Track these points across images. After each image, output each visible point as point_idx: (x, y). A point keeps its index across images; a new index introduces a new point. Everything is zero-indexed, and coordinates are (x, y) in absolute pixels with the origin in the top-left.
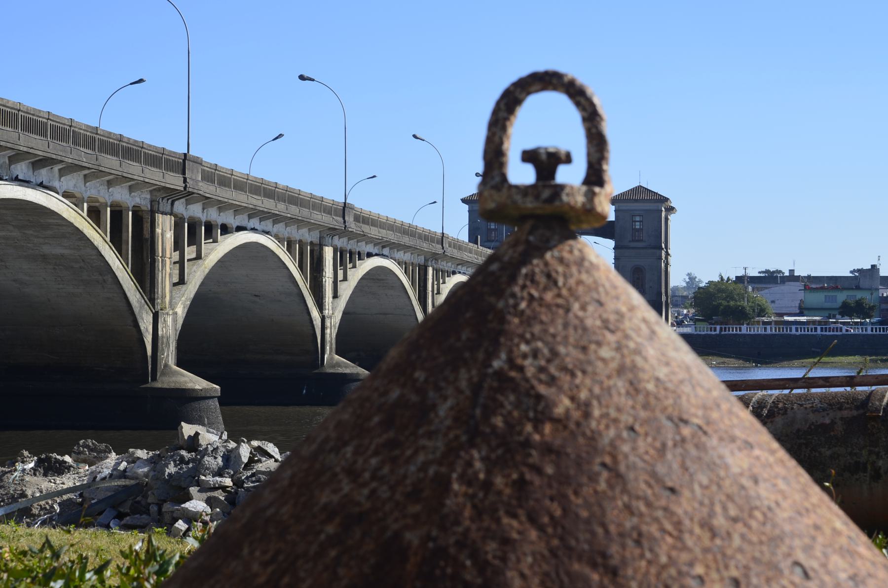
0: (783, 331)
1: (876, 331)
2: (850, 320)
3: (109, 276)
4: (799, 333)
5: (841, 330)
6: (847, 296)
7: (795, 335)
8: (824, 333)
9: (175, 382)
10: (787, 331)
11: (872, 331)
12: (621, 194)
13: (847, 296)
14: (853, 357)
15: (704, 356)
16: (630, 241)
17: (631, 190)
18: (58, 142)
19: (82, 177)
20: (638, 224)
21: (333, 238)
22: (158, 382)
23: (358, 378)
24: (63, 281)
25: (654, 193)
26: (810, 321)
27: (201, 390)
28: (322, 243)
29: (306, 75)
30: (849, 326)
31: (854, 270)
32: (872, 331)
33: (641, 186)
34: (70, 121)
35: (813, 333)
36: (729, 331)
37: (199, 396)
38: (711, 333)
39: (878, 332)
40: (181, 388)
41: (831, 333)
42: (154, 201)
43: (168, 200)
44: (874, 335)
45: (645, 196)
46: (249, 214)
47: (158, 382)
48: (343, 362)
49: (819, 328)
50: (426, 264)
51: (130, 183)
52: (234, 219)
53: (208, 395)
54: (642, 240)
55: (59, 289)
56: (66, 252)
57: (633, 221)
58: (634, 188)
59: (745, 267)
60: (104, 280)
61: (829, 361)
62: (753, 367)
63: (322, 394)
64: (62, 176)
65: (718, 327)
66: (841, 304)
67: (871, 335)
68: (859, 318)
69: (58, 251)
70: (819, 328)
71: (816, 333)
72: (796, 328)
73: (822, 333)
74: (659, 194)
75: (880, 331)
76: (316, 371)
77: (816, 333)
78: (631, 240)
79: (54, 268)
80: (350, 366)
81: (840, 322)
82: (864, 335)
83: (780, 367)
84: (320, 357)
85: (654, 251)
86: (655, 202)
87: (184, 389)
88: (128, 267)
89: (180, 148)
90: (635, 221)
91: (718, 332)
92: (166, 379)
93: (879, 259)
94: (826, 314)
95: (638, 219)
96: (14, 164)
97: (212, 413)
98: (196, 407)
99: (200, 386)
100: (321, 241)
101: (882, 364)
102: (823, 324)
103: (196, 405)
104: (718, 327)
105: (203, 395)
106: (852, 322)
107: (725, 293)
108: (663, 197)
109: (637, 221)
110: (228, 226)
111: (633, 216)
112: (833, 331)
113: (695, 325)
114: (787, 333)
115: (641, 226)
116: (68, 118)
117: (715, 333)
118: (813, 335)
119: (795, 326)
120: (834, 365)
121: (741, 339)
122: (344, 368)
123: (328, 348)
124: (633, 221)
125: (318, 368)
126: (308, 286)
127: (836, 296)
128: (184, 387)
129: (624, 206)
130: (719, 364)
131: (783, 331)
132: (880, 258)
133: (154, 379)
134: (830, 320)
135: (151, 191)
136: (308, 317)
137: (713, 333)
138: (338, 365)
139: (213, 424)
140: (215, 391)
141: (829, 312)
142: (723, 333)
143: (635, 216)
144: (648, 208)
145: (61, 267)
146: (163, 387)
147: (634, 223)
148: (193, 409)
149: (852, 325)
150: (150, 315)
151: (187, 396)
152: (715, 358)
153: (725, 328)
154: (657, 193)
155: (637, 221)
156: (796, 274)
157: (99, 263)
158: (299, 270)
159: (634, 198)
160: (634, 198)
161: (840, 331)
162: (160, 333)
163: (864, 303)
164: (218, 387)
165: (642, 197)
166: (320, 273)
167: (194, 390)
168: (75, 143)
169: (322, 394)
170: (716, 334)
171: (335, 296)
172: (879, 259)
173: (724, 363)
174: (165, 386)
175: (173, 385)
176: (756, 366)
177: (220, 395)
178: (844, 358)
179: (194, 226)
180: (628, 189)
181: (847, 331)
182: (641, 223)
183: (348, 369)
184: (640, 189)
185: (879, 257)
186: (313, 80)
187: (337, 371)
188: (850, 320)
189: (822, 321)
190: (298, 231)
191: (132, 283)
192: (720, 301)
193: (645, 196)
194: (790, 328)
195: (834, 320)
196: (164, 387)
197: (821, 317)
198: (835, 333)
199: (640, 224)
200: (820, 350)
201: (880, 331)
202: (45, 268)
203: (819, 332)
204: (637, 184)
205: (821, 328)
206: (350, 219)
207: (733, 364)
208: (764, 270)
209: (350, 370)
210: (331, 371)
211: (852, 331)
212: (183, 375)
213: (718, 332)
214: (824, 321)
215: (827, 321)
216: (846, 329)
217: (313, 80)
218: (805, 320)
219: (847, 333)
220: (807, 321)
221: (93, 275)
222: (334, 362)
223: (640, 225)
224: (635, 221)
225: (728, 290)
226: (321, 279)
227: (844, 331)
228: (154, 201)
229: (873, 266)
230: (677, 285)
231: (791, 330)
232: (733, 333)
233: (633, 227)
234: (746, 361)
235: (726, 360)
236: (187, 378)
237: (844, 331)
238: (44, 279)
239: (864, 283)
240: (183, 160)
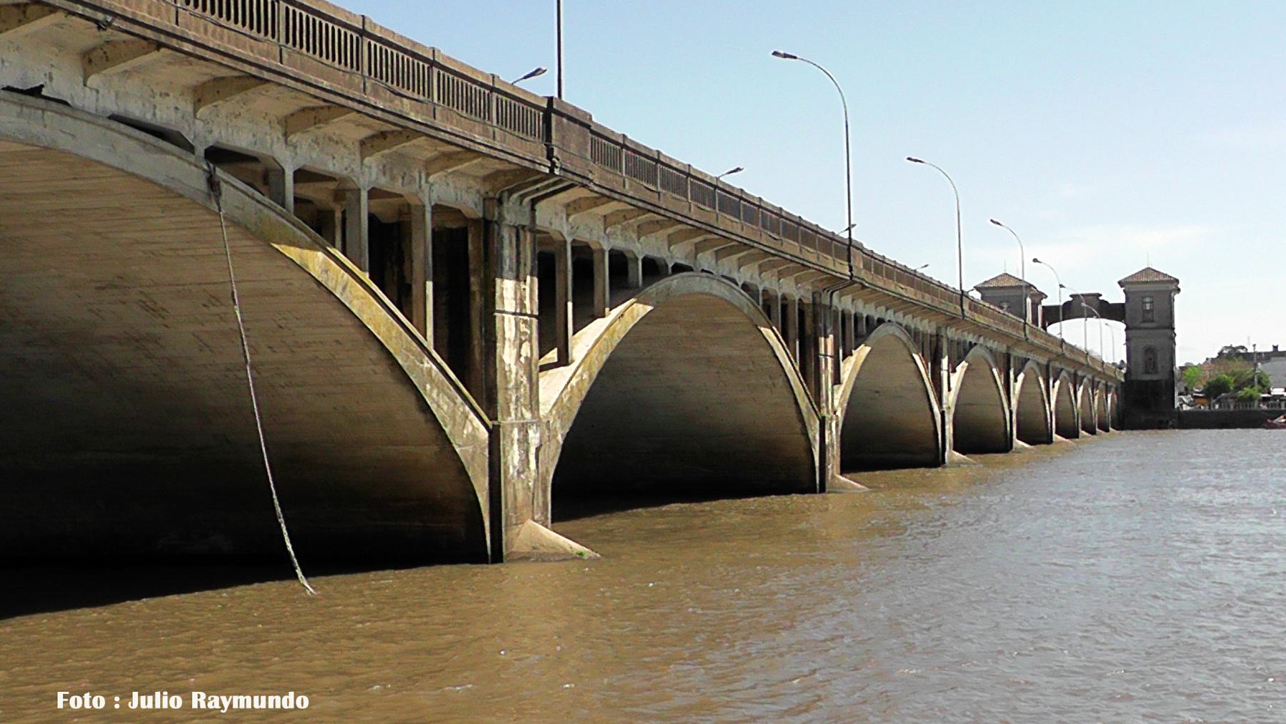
16: (1141, 322)
18: (223, 21)
19: (757, 266)
21: (538, 207)
34: (491, 78)
43: (523, 197)
51: (670, 231)
56: (736, 353)
63: (651, 585)
79: (718, 373)
88: (425, 336)
89: (541, 89)
90: (1146, 303)
96: (702, 252)
110: (628, 255)
116: (488, 72)
126: (797, 368)
129: (1133, 288)
158: (780, 337)
162: (827, 441)
168: (764, 226)
169: (651, 585)
171: (949, 390)
179: (584, 258)
184: (1148, 271)
204: (1146, 267)
206: (858, 263)
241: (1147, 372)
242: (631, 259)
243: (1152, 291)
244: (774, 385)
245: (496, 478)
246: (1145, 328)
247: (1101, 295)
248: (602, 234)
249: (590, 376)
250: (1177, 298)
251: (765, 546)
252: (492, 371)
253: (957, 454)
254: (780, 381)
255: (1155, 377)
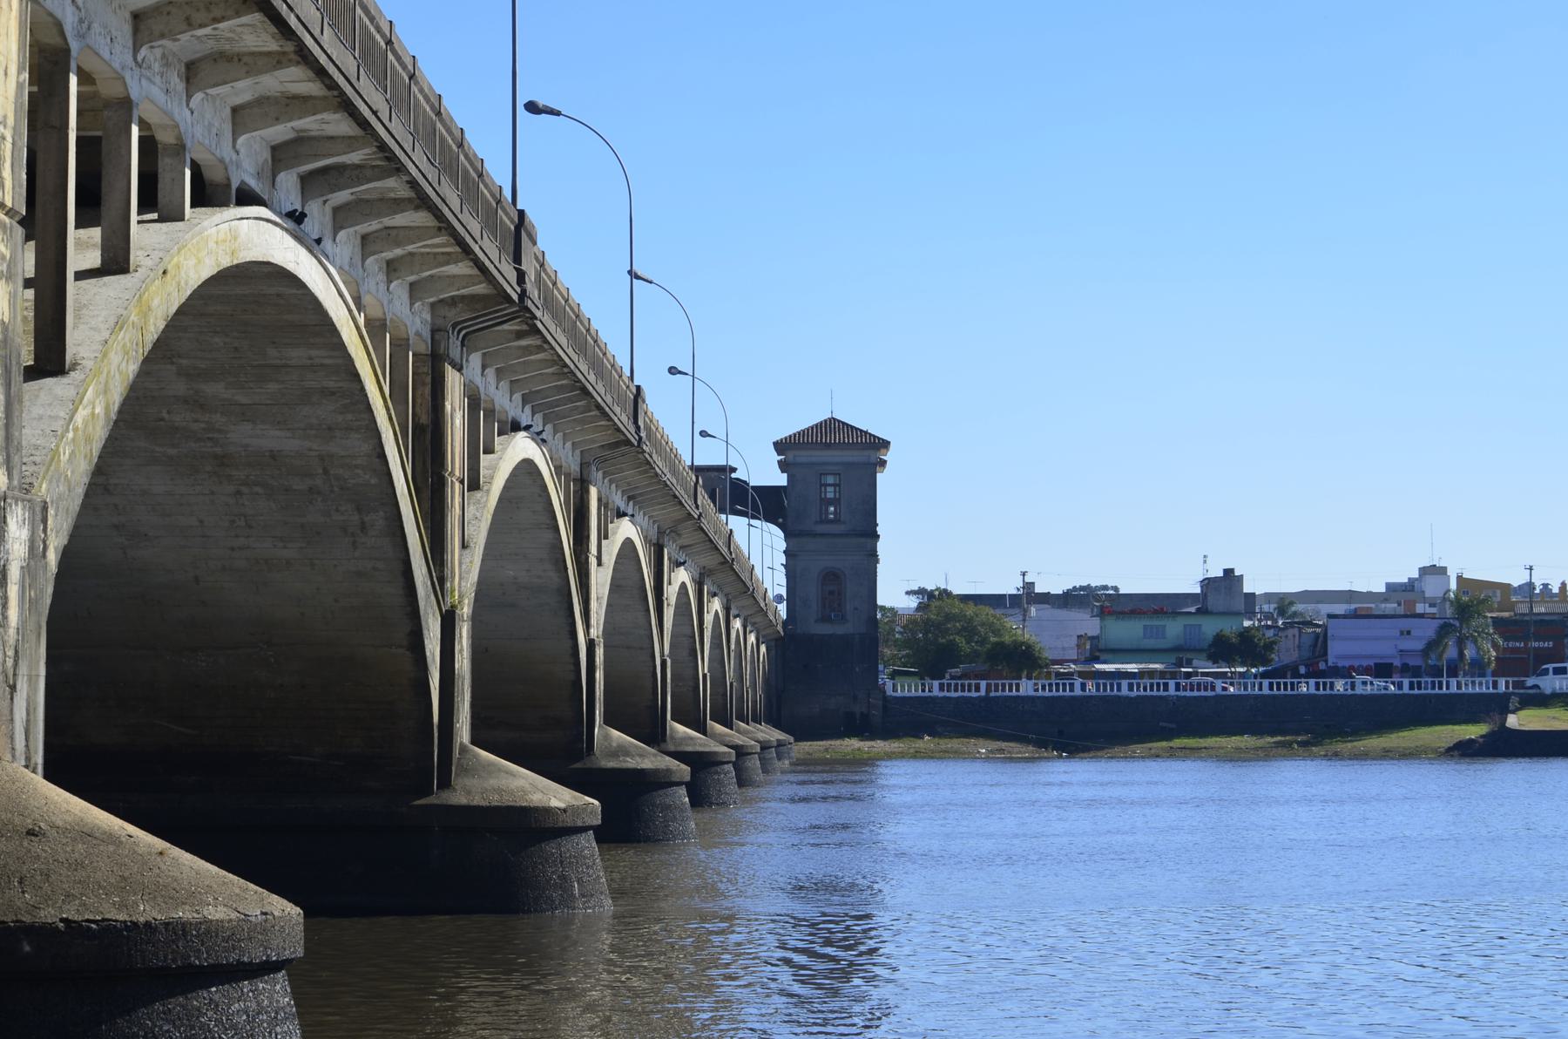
0: (1105, 690)
1: (1278, 689)
2: (1228, 670)
3: (381, 513)
4: (1135, 693)
5: (1213, 688)
6: (1185, 626)
7: (1127, 698)
8: (1182, 693)
9: (499, 791)
10: (1112, 690)
11: (1318, 689)
12: (799, 433)
13: (1185, 626)
14: (1238, 738)
15: (960, 737)
16: (816, 523)
17: (817, 425)
20: (830, 489)
22: (455, 790)
23: (668, 780)
24: (250, 527)
25: (861, 431)
26: (1144, 672)
27: (565, 811)
28: (585, 477)
29: (542, 101)
30: (1228, 681)
31: (1075, 587)
32: (1271, 688)
33: (834, 419)
35: (1162, 693)
36: (1003, 690)
37: (560, 825)
38: (948, 694)
39: (1275, 691)
40: (518, 805)
41: (1196, 693)
42: (439, 330)
44: (1274, 696)
45: (844, 437)
46: (523, 394)
47: (455, 790)
48: (632, 743)
49: (1172, 683)
50: (661, 542)
52: (511, 400)
53: (579, 824)
54: (839, 520)
55: (232, 549)
57: (821, 485)
58: (821, 423)
59: (1024, 571)
60: (363, 523)
61: (1200, 746)
62: (1054, 758)
64: (342, 228)
65: (983, 684)
66: (1211, 639)
67: (1268, 696)
68: (1243, 664)
69: (270, 438)
70: (1172, 683)
71: (1166, 693)
72: (1129, 683)
73: (1178, 693)
74: (870, 435)
75: (1286, 689)
76: (578, 765)
77: (1166, 693)
78: (818, 520)
79: (239, 493)
80: (649, 753)
81: (1201, 672)
82: (1256, 697)
83: (1109, 757)
84: (436, 735)
85: (862, 540)
86: (863, 449)
87: (525, 807)
90: (827, 485)
91: (983, 693)
92: (471, 782)
93: (1205, 562)
94: (1172, 658)
95: (830, 480)
97: (587, 868)
98: (553, 854)
99: (560, 800)
100: (585, 473)
101: (1301, 750)
102: (1168, 676)
103: (551, 848)
104: (983, 684)
105: (569, 821)
106: (1231, 672)
107: (959, 621)
108: (879, 438)
109: (830, 485)
111: (821, 474)
112: (1199, 690)
113: (894, 679)
114: (1112, 694)
115: (837, 494)
117: (977, 694)
118: (1161, 697)
119: (1128, 681)
120: (1212, 752)
121: (1026, 707)
122: (638, 758)
123: (597, 712)
124: (839, 485)
125: (583, 759)
127: (1165, 626)
128: (525, 804)
129: (804, 456)
130: (991, 752)
131: (1105, 690)
132: (1207, 559)
133: (445, 783)
134: (1183, 670)
135: (433, 305)
136: (570, 643)
137: (974, 694)
138: (622, 751)
139: (592, 895)
140: (591, 813)
141: (1181, 652)
142: (993, 694)
143: (824, 474)
144: (850, 459)
145: (258, 489)
146: (472, 804)
147: (823, 488)
148: (547, 861)
149: (1232, 678)
150: (437, 619)
151: (534, 826)
152: (981, 741)
153: (996, 686)
154: (866, 433)
155: (830, 485)
156: (1038, 589)
157: (367, 477)
159: (824, 440)
160: (824, 440)
161: (1211, 690)
163: (1255, 637)
164: (596, 802)
165: (839, 439)
166: (581, 545)
167: (548, 811)
170: (979, 697)
172: (1205, 562)
173: (1001, 751)
174: (477, 801)
175: (496, 797)
176: (1060, 757)
177: (600, 822)
178: (1223, 740)
180: (807, 427)
181: (1225, 689)
182: (837, 488)
183: (646, 761)
185: (1205, 556)
186: (558, 113)
187: (625, 765)
188: (1228, 670)
189: (1166, 672)
190: (564, 444)
191: (417, 534)
192: (951, 637)
193: (844, 437)
194: (1117, 683)
195: (1190, 670)
196: (475, 803)
197: (1162, 663)
198: (1203, 693)
199: (835, 489)
200: (1174, 726)
201: (1286, 689)
202: (213, 493)
203: (1172, 691)
204: (827, 416)
205: (1316, 682)
207: (1017, 753)
208: (916, 589)
209: (652, 762)
210: (612, 764)
211: (1232, 689)
212: (500, 769)
213: (983, 693)
214: (1170, 672)
215: (1176, 672)
216: (1223, 687)
217: (558, 113)
218: (1136, 671)
219: (1224, 693)
220: (1140, 672)
221: (337, 510)
222: (614, 744)
223: (835, 492)
224: (827, 485)
225: (965, 616)
226: (583, 557)
227: (1219, 690)
228: (439, 330)
229: (1229, 572)
230: (1404, 572)
231: (1119, 689)
232: (1011, 694)
233: (820, 496)
234: (1040, 747)
235: (1004, 745)
236: (524, 781)
237: (1219, 690)
238: (201, 522)
239: (1214, 602)
240: (515, 228)
241: (825, 619)
242: (166, 147)
243: (837, 464)
244: (363, 527)
245: (658, 565)
246: (822, 535)
247: (734, 470)
248: (129, 58)
249: (107, 408)
250: (885, 482)
251: (1046, 923)
252: (419, 188)
253: (615, 733)
254: (378, 519)
255: (840, 630)
